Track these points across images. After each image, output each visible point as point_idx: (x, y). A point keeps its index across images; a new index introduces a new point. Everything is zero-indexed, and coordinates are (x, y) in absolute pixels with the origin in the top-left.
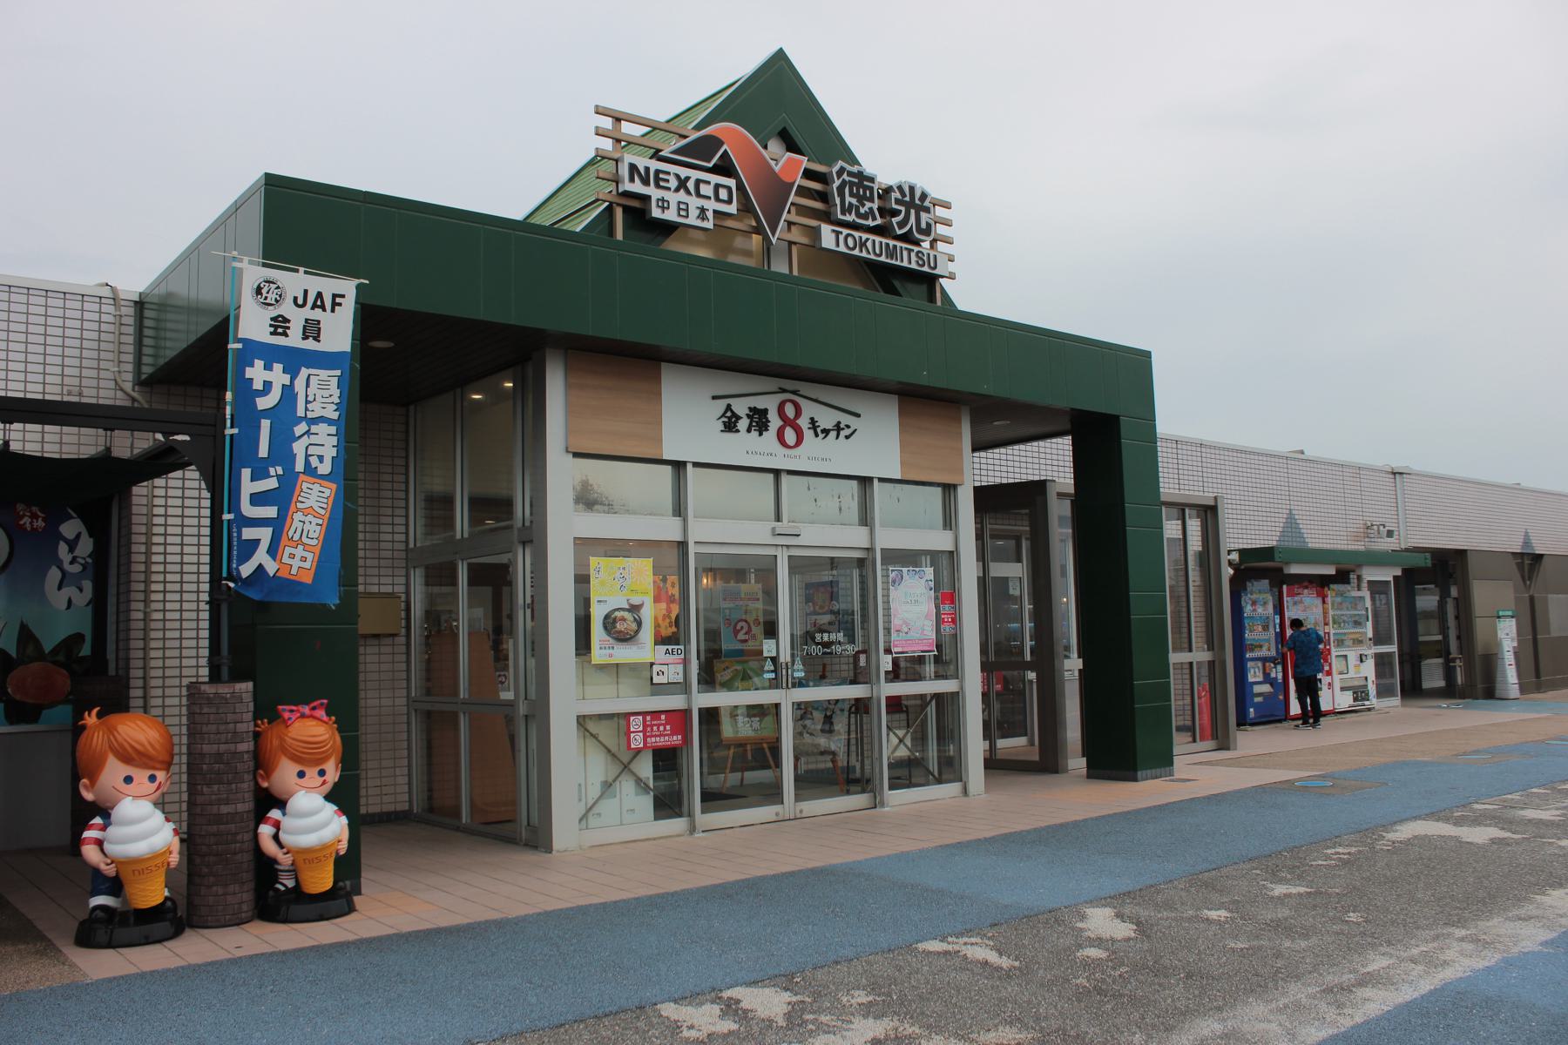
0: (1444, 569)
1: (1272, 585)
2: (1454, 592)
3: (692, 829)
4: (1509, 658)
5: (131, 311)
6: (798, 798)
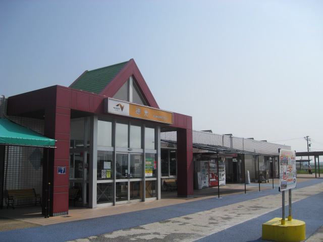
0: (241, 156)
1: (215, 161)
2: (241, 161)
3: (114, 205)
4: (249, 175)
5: (154, 156)
6: (130, 199)
